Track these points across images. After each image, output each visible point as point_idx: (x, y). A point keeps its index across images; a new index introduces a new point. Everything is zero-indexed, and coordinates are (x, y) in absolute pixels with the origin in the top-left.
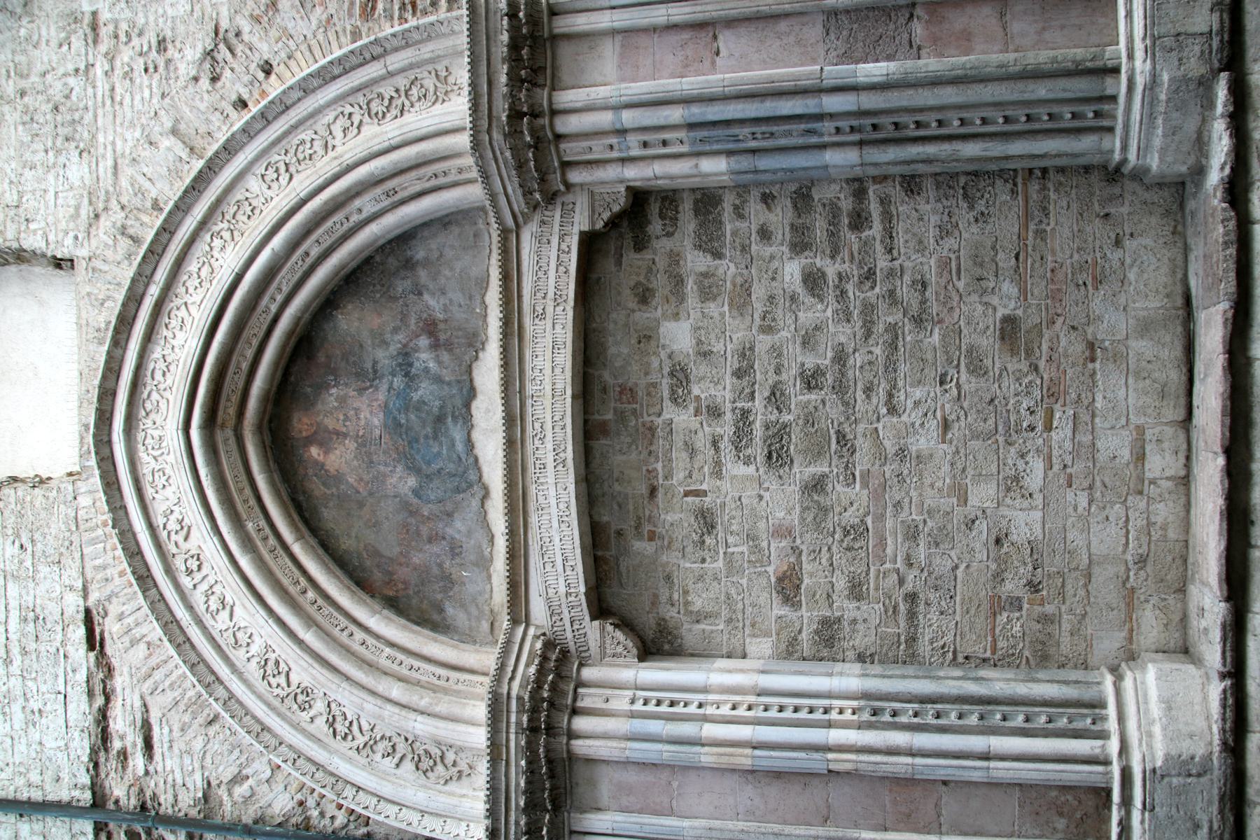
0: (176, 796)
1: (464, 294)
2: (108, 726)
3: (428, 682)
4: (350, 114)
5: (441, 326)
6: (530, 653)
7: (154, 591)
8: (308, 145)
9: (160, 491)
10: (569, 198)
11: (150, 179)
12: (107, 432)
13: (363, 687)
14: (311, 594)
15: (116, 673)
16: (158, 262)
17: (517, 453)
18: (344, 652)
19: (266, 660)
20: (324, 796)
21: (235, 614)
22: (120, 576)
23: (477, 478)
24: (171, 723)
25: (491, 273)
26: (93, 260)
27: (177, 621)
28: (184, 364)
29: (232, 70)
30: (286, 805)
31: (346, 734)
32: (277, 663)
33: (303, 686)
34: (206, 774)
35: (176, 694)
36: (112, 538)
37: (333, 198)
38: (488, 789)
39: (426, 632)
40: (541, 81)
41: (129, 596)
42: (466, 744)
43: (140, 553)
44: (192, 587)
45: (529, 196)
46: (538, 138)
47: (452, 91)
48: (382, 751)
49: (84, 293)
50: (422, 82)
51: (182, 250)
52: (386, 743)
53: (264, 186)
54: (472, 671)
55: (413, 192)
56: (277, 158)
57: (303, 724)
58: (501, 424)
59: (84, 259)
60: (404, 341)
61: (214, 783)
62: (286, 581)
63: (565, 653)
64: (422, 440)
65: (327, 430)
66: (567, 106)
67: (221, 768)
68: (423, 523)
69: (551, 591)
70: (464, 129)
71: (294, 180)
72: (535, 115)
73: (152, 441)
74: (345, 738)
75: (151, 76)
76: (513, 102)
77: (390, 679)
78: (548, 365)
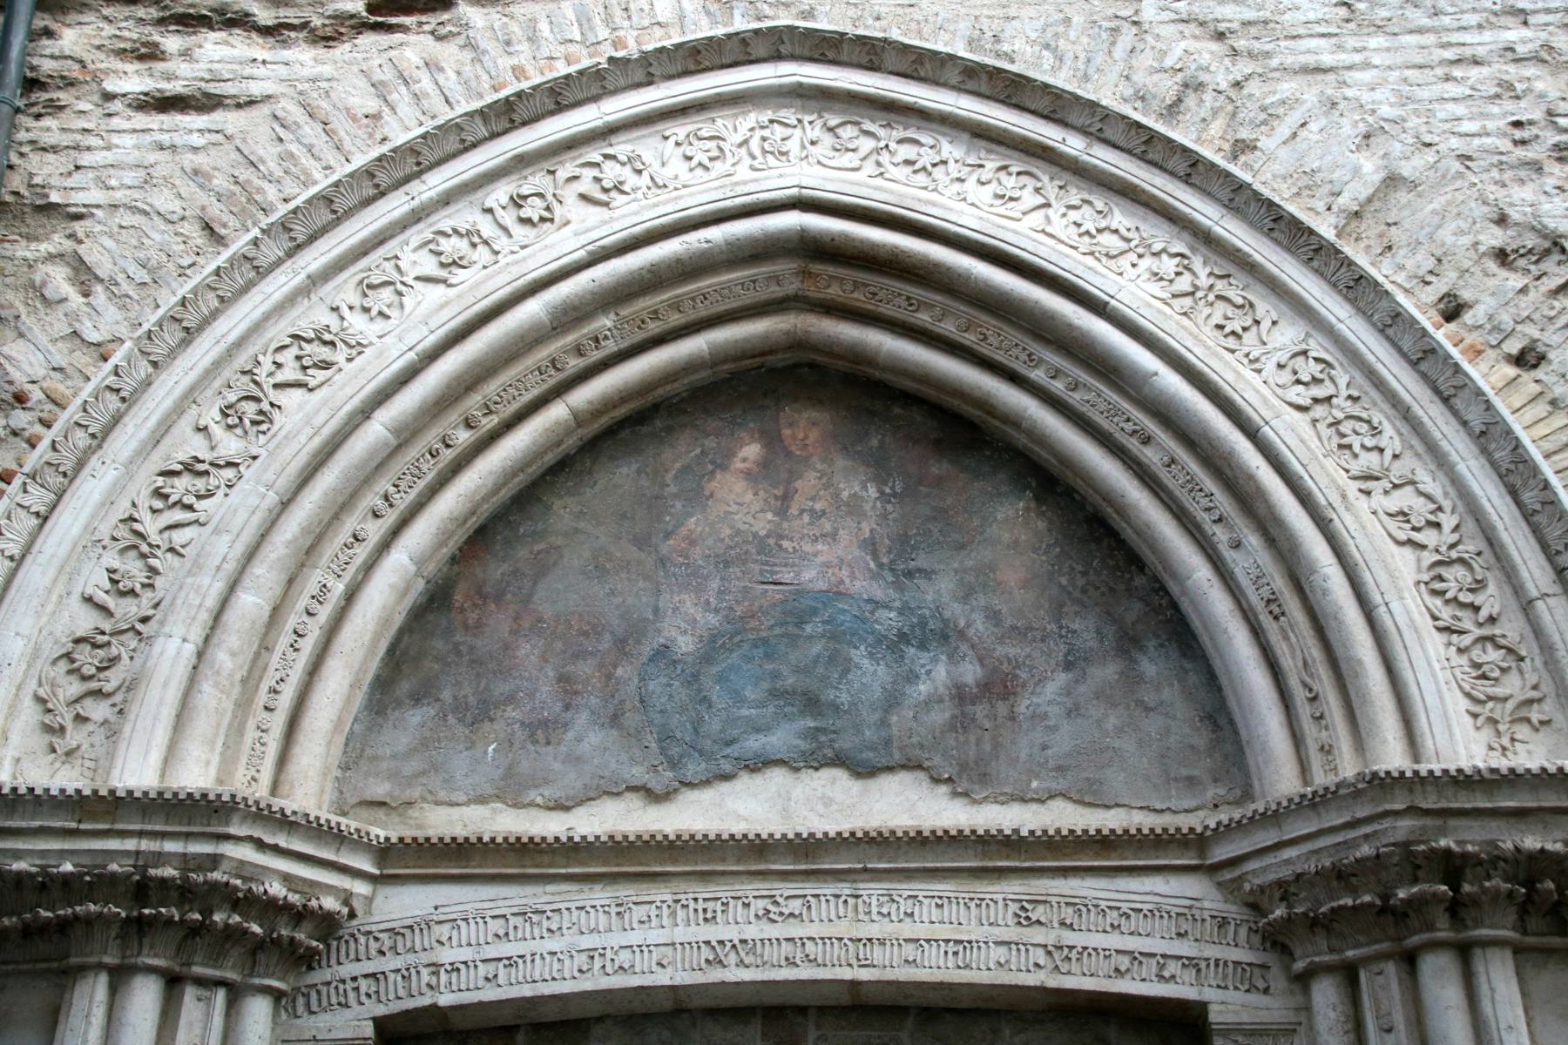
0: (54, 149)
1: (1068, 755)
2: (212, 28)
3: (265, 669)
4: (1437, 525)
5: (1002, 708)
6: (313, 884)
7: (483, 131)
8: (1369, 442)
9: (680, 151)
10: (1278, 981)
11: (1295, 135)
12: (798, 51)
13: (264, 536)
14: (463, 437)
15: (320, 51)
16: (1129, 152)
17: (739, 861)
18: (341, 500)
19: (332, 344)
20: (33, 446)
21: (430, 287)
22: (514, 69)
23: (689, 779)
24: (213, 151)
25: (1113, 812)
26: (1134, 30)
27: (419, 174)
28: (928, 202)
29: (1523, 290)
30: (19, 368)
31: (166, 497)
32: (325, 365)
33: (276, 414)
34: (99, 213)
35: (272, 165)
36: (591, 56)
37: (1261, 492)
38: (14, 790)
39: (374, 666)
40: (1533, 923)
41: (473, 84)
42: (123, 746)
43: (560, 108)
44: (488, 205)
45: (1277, 895)
46: (1406, 915)
47: (1498, 734)
48: (122, 568)
49: (1069, 11)
50: (1514, 672)
51: (1154, 197)
52: (141, 577)
53: (1283, 357)
54: (283, 760)
55: (1279, 652)
56: (1343, 380)
57: (194, 410)
58: (799, 829)
59: (1137, 12)
60: (971, 632)
61: (79, 227)
62: (492, 388)
63: (307, 960)
64: (769, 667)
65: (793, 475)
66: (1482, 980)
67: (109, 243)
68: (601, 666)
69: (444, 931)
70: (1416, 758)
71: (1297, 415)
72: (1456, 909)
73: (778, 137)
74: (158, 493)
75: (1505, 135)
76: (1480, 863)
77: (278, 591)
78: (922, 931)
